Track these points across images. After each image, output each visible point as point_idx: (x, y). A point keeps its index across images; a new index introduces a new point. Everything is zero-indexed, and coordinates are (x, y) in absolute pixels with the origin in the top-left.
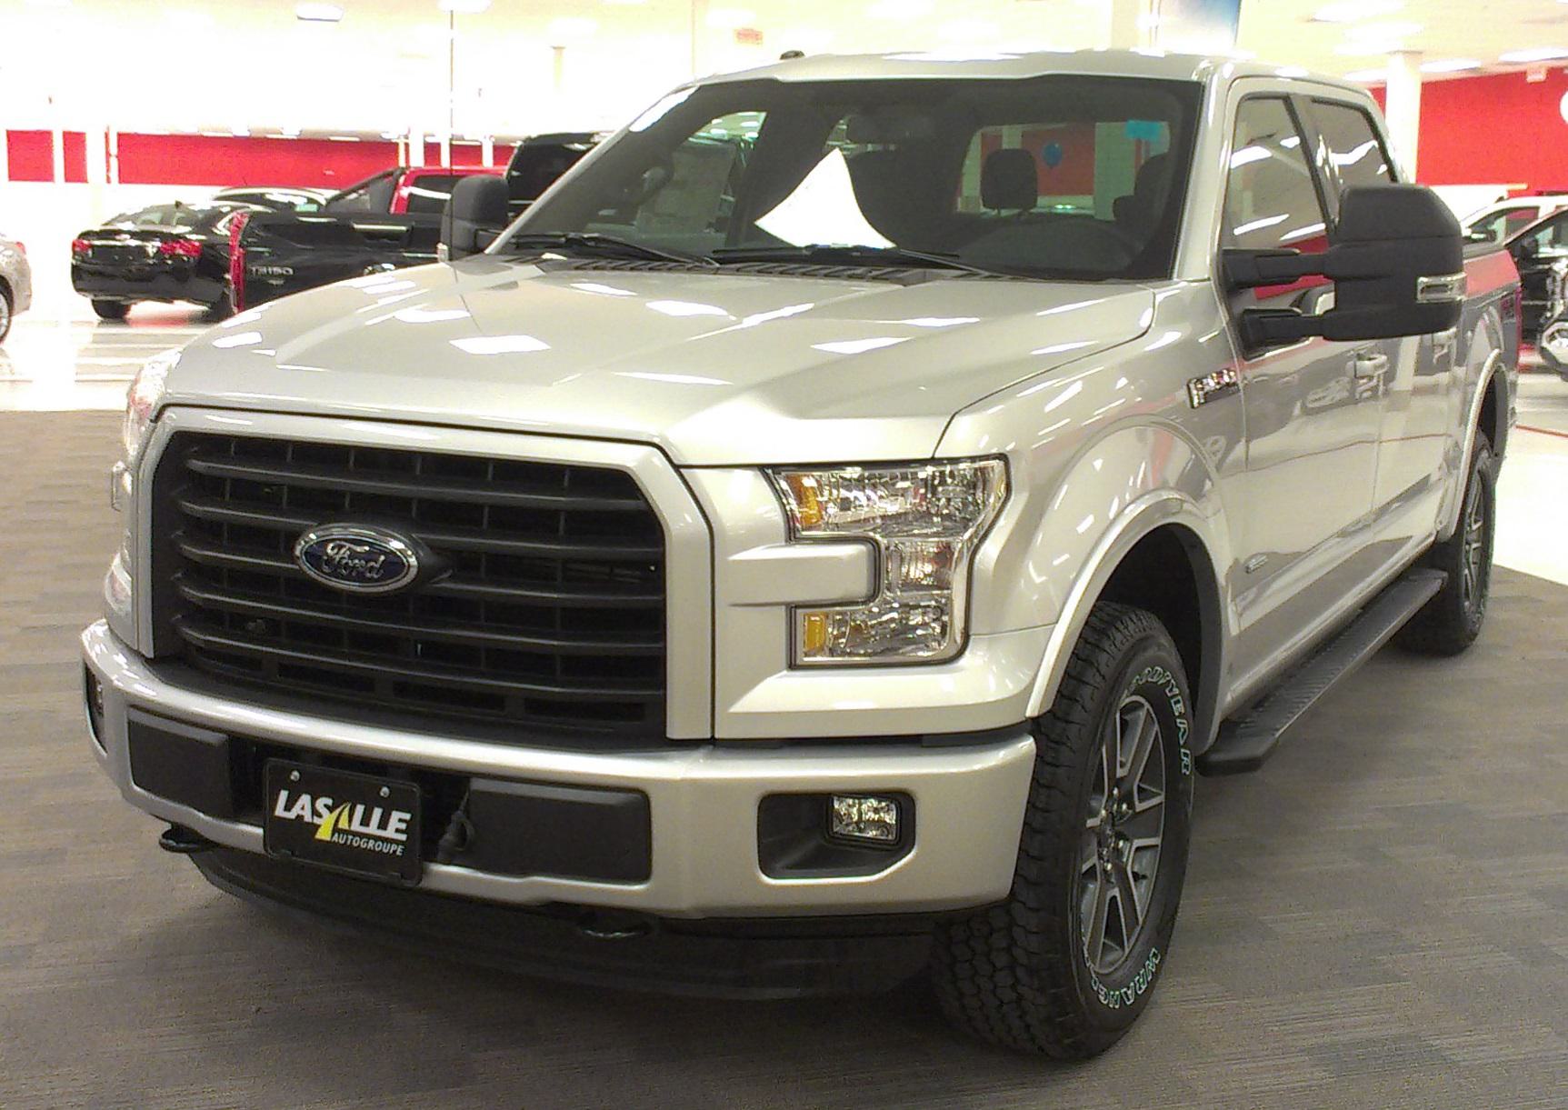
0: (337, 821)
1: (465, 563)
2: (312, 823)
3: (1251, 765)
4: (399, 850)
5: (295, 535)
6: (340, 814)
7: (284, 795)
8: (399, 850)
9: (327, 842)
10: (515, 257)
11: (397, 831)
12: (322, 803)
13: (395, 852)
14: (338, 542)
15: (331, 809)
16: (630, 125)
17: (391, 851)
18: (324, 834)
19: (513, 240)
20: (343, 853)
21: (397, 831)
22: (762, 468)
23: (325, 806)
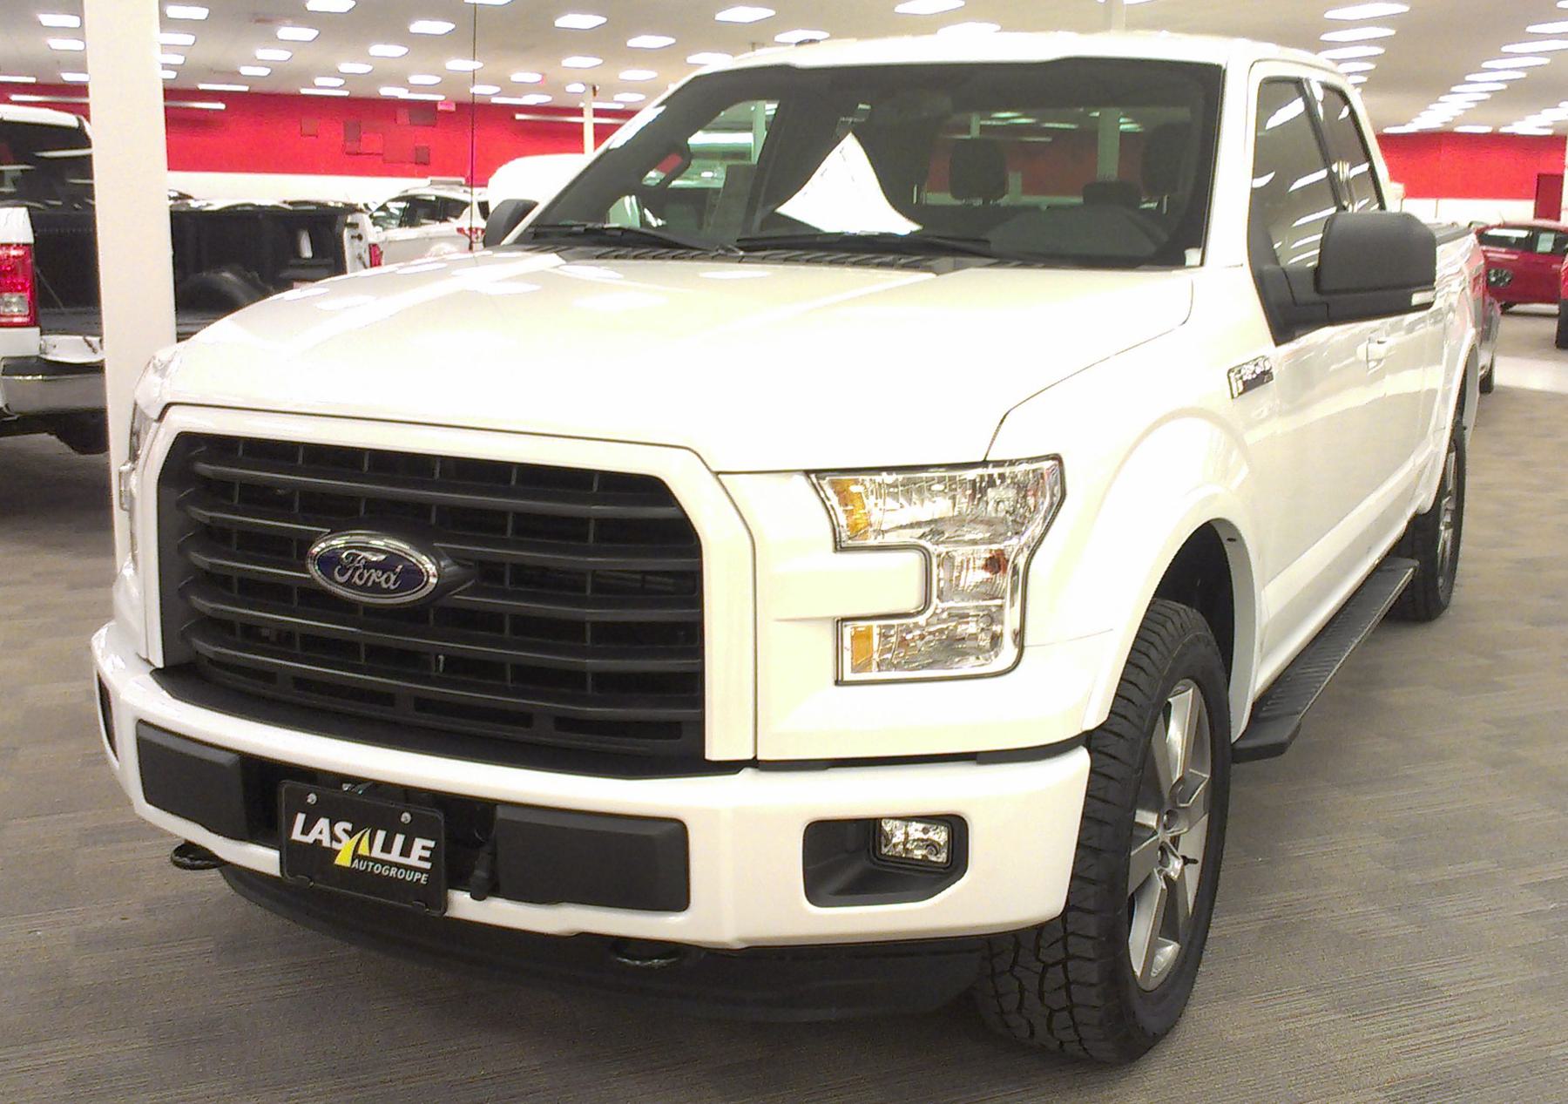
1: (489, 574)
2: (331, 848)
3: (1277, 750)
4: (424, 878)
5: (311, 540)
6: (360, 840)
7: (301, 818)
9: (348, 868)
10: (536, 246)
11: (421, 858)
12: (340, 827)
13: (419, 880)
14: (354, 551)
15: (351, 834)
17: (415, 880)
18: (344, 859)
19: (532, 230)
20: (361, 879)
21: (421, 858)
22: (807, 473)
23: (345, 830)
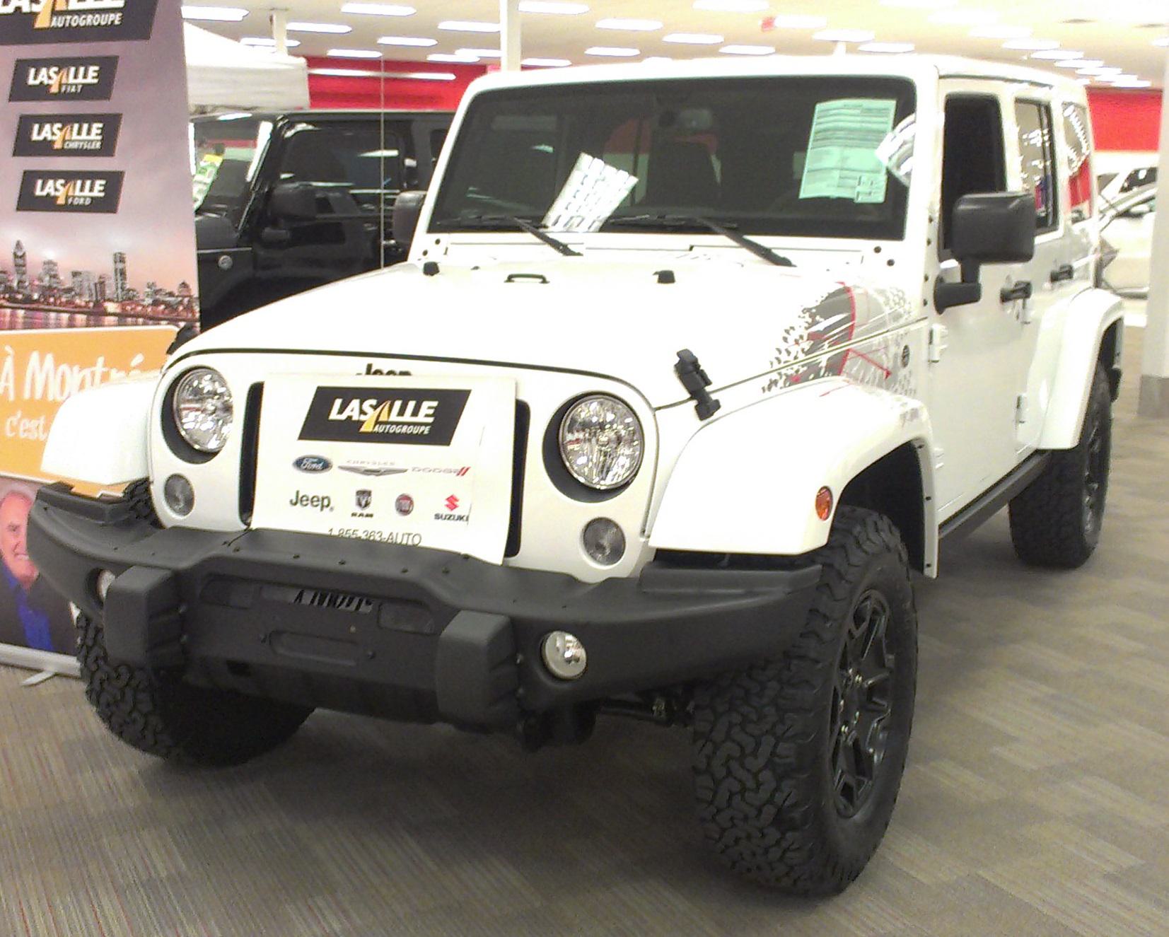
0: (379, 416)
8: (118, 19)
16: (571, 244)
17: (109, 23)
